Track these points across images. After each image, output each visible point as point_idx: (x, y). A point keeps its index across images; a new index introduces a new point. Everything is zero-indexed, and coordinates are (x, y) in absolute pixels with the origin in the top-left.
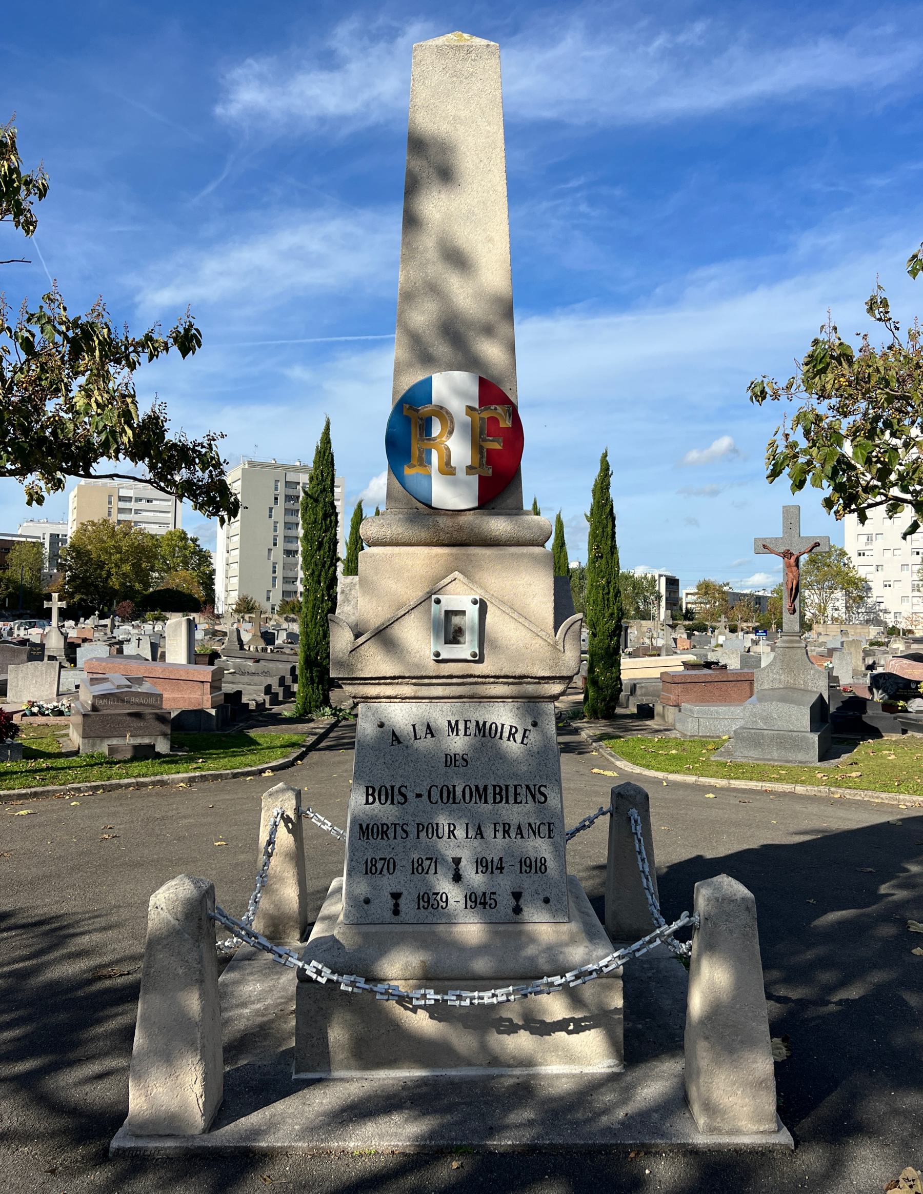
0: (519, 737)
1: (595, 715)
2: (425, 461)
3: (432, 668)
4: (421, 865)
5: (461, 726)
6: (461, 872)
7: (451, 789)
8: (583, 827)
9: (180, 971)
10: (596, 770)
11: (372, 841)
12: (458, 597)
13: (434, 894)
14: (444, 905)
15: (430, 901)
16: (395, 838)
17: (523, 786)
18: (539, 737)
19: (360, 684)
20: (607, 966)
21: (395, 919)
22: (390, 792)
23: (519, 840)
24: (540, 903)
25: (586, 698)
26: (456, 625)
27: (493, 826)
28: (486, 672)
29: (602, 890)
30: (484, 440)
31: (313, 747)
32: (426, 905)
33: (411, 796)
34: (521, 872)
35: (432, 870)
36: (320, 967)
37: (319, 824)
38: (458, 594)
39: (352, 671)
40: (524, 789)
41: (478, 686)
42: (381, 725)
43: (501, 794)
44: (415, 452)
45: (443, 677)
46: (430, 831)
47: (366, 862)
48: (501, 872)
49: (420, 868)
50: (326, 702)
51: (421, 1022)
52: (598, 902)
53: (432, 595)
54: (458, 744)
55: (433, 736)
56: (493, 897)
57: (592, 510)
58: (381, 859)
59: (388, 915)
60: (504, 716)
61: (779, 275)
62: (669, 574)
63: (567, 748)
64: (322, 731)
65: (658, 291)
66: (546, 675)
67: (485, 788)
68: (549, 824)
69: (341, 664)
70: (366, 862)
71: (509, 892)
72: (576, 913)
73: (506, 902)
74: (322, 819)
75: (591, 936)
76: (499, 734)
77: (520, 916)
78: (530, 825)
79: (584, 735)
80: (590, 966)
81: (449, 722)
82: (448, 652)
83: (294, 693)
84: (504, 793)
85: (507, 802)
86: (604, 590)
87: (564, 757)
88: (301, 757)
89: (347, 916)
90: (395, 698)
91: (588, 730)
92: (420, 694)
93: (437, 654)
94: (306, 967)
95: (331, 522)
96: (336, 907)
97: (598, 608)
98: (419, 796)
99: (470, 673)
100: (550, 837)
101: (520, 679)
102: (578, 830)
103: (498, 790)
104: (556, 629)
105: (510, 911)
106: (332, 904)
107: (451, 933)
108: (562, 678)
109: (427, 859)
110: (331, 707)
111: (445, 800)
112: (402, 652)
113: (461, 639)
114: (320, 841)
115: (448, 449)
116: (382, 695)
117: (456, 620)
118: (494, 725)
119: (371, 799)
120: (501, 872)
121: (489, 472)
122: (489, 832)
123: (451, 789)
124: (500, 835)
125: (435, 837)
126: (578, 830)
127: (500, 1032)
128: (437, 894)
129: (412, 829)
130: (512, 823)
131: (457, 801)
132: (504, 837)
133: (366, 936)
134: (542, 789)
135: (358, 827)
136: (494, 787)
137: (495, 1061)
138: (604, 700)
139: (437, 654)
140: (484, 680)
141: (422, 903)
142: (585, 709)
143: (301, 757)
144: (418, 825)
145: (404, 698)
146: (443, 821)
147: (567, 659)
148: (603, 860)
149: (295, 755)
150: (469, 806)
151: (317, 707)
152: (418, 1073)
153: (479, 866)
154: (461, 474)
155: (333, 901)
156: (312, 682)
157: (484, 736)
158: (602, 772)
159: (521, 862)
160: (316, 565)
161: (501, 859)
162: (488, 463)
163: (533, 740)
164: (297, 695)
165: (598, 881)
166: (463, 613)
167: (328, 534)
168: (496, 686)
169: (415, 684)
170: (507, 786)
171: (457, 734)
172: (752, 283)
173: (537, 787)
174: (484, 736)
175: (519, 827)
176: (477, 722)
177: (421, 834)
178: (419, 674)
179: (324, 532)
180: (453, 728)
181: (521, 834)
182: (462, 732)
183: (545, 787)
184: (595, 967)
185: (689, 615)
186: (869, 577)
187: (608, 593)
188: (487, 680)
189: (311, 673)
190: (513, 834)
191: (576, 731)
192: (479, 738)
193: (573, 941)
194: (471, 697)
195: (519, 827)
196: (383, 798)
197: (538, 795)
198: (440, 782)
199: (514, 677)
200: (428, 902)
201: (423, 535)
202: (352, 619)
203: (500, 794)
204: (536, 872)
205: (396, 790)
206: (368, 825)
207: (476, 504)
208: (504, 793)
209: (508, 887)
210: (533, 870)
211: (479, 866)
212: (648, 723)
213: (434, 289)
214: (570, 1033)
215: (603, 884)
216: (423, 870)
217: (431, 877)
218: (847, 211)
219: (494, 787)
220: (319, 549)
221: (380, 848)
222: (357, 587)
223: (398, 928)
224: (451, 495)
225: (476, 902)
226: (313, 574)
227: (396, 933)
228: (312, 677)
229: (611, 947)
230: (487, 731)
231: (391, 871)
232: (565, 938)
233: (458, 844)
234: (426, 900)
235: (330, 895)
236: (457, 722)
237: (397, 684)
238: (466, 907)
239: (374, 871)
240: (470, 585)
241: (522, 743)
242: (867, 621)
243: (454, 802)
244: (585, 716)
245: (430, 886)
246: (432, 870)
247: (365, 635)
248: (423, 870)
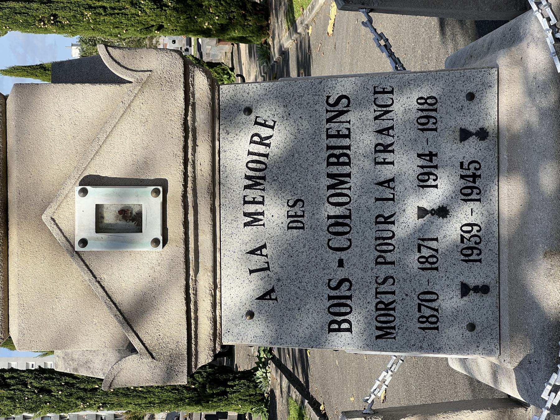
0: (265, 132)
1: (263, 29)
4: (427, 258)
5: (251, 208)
6: (435, 207)
7: (332, 221)
8: (387, 47)
10: (330, 30)
11: (396, 323)
12: (77, 214)
13: (462, 241)
14: (476, 228)
15: (471, 248)
16: (393, 293)
17: (328, 126)
18: (265, 106)
19: (196, 345)
20: (549, 20)
21: (494, 291)
22: (336, 301)
24: (473, 105)
25: (242, 40)
26: (117, 217)
27: (378, 166)
28: (179, 177)
29: (468, 23)
31: (304, 390)
32: (476, 252)
33: (341, 274)
34: (436, 130)
35: (434, 244)
36: (549, 388)
37: (384, 387)
38: (73, 214)
39: (178, 356)
40: (332, 125)
41: (198, 187)
42: (251, 314)
43: (338, 156)
45: (186, 233)
46: (384, 248)
47: (424, 329)
48: (436, 155)
49: (431, 260)
50: (249, 375)
52: (483, 28)
53: (77, 250)
54: (275, 212)
55: (264, 246)
56: (465, 166)
58: (419, 311)
59: (489, 300)
60: (237, 151)
63: (305, 65)
64: (285, 381)
66: (182, 95)
67: (330, 176)
68: (376, 93)
69: (170, 371)
70: (424, 329)
71: (461, 145)
72: (488, 58)
73: (472, 149)
74: (378, 383)
75: (514, 39)
76: (262, 159)
77: (490, 130)
78: (376, 118)
79: (289, 44)
80: (548, 40)
81: (246, 225)
82: (152, 227)
83: (239, 416)
84: (337, 152)
85: (348, 148)
86: (100, 14)
87: (316, 71)
88: (315, 405)
89: (490, 353)
90: (214, 297)
91: (282, 39)
92: (210, 264)
93: (156, 242)
94: (549, 405)
95: (12, 378)
96: (482, 365)
97: (125, 21)
98: (341, 263)
99: (180, 199)
100: (392, 92)
101: (188, 131)
102: (391, 55)
103: (333, 160)
104: (120, 81)
105: (483, 144)
106: (479, 370)
107: (510, 219)
108: (187, 74)
109: (419, 251)
110: (256, 369)
111: (347, 229)
112: (152, 290)
113: (135, 210)
114: (412, 381)
116: (210, 315)
117: (110, 218)
118: (250, 165)
119: (345, 326)
120: (436, 155)
122: (387, 172)
123: (332, 221)
124: (389, 157)
125: (392, 241)
126: (391, 55)
128: (462, 237)
130: (375, 142)
131: (347, 213)
132: (393, 151)
133: (515, 329)
134: (331, 101)
135: (379, 341)
136: (329, 164)
138: (244, 16)
139: (156, 242)
140: (190, 179)
141: (474, 257)
142: (257, 42)
143: (315, 405)
144: (377, 263)
145: (215, 286)
147: (161, 67)
148: (434, 21)
149: (313, 413)
150: (354, 197)
151: (256, 386)
153: (428, 183)
155: (475, 368)
156: (225, 393)
157: (263, 178)
158: (331, 22)
159: (422, 130)
160: (71, 395)
161: (419, 156)
163: (268, 113)
164: (242, 412)
165: (458, 30)
166: (99, 208)
167: (29, 381)
168: (198, 163)
169: (197, 271)
170: (329, 148)
171: (262, 214)
173: (329, 108)
174: (263, 178)
175: (380, 132)
176: (246, 187)
177: (389, 260)
178: (183, 266)
179: (25, 385)
180: (253, 219)
181: (388, 129)
183: (328, 97)
184: (550, 34)
187: (104, 8)
188: (190, 174)
189: (212, 396)
190: (389, 140)
191: (284, 53)
192: (266, 185)
193: (521, 62)
194: (213, 196)
195: (380, 132)
196: (343, 310)
197: (340, 107)
199: (186, 138)
200: (472, 248)
202: (112, 356)
203: (338, 157)
204: (435, 110)
205: (333, 293)
206: (378, 328)
208: (337, 152)
209: (454, 147)
210: (433, 114)
211: (428, 183)
215: (462, 23)
216: (432, 256)
217: (441, 246)
219: (329, 164)
220: (49, 392)
221: (406, 312)
222: (69, 351)
223: (505, 287)
225: (472, 188)
226: (83, 400)
227: (511, 289)
228: (218, 394)
229: (528, 13)
230: (258, 174)
231: (434, 297)
232: (517, 72)
234: (469, 252)
235: (469, 372)
236: (246, 214)
237: (195, 295)
238: (479, 200)
239: (434, 319)
240: (60, 199)
241: (272, 127)
243: (349, 217)
244: (266, 42)
245: (450, 250)
246: (434, 244)
247: (131, 340)
248: (432, 256)
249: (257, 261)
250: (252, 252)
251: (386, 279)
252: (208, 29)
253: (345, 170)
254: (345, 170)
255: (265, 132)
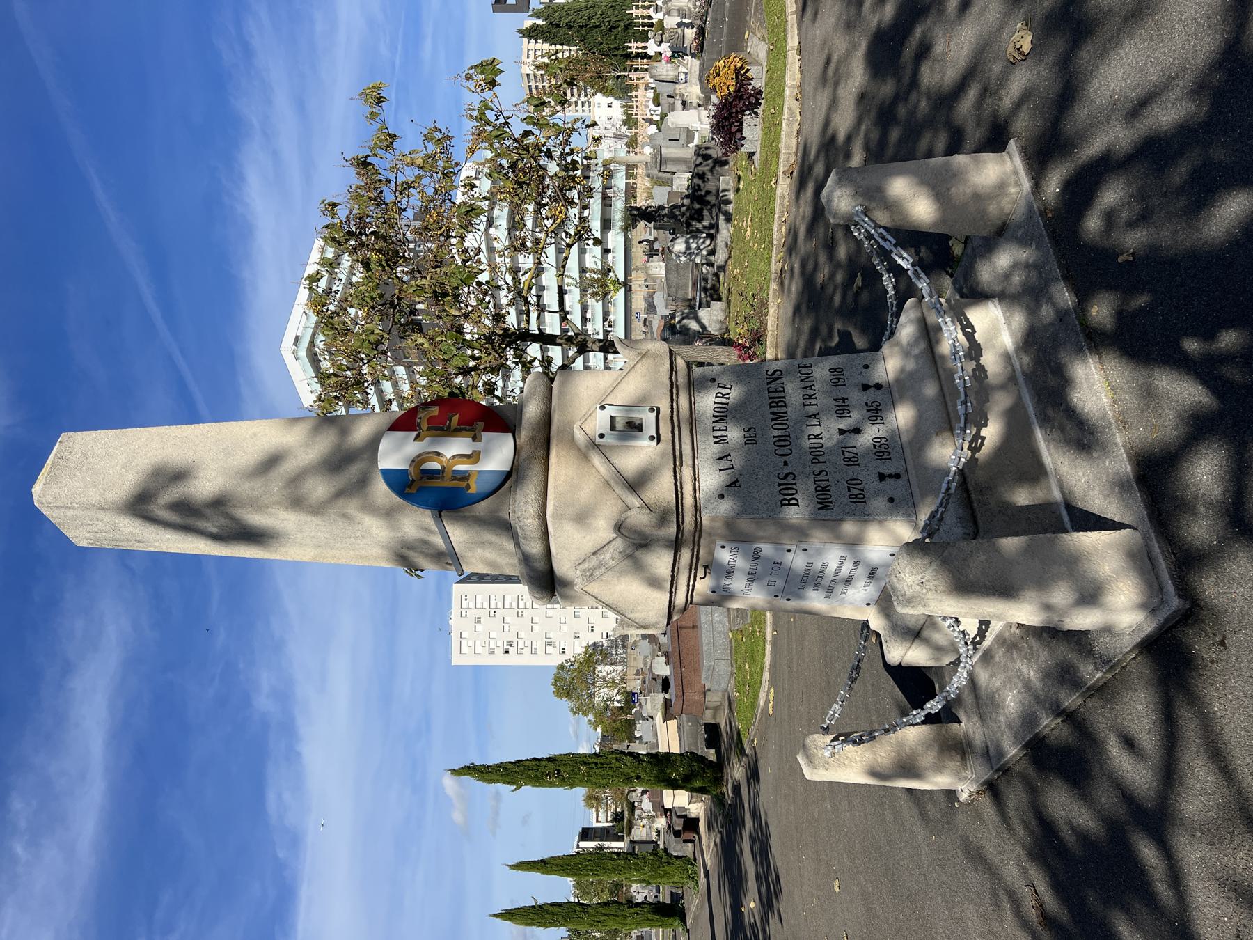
0: (725, 391)
2: (465, 476)
3: (666, 445)
5: (719, 433)
9: (983, 557)
11: (833, 499)
15: (882, 450)
21: (904, 477)
23: (817, 387)
30: (449, 426)
33: (786, 470)
44: (455, 484)
51: (992, 432)
54: (735, 434)
57: (509, 783)
59: (901, 483)
60: (708, 402)
61: (289, 729)
62: (577, 838)
65: (281, 854)
73: (872, 395)
92: (690, 463)
93: (652, 438)
98: (786, 463)
101: (673, 386)
105: (880, 392)
107: (907, 431)
115: (454, 457)
117: (620, 425)
121: (481, 424)
122: (812, 410)
127: (986, 377)
129: (818, 467)
137: (1012, 379)
146: (807, 443)
152: (1039, 434)
154: (478, 446)
162: (471, 424)
166: (612, 419)
169: (681, 465)
172: (293, 756)
182: (724, 433)
185: (618, 817)
186: (584, 644)
190: (812, 392)
198: (771, 447)
201: (536, 469)
207: (510, 436)
212: (722, 726)
213: (296, 480)
214: (974, 331)
218: (241, 666)
221: (838, 492)
223: (912, 472)
224: (498, 454)
233: (827, 430)
242: (624, 646)
246: (854, 450)
249: (724, 464)
250: (721, 459)
251: (820, 473)
252: (675, 780)
253: (784, 409)
254: (784, 409)
255: (725, 391)
